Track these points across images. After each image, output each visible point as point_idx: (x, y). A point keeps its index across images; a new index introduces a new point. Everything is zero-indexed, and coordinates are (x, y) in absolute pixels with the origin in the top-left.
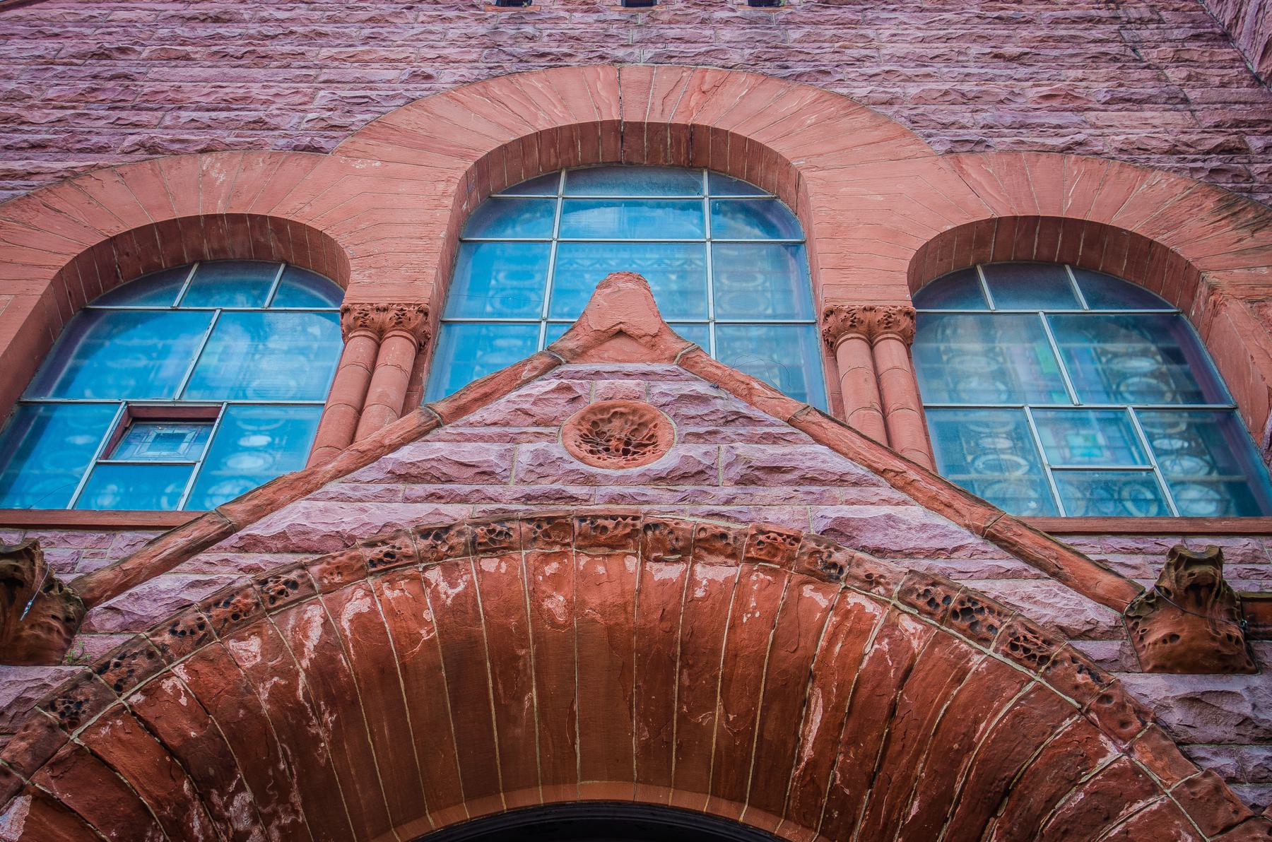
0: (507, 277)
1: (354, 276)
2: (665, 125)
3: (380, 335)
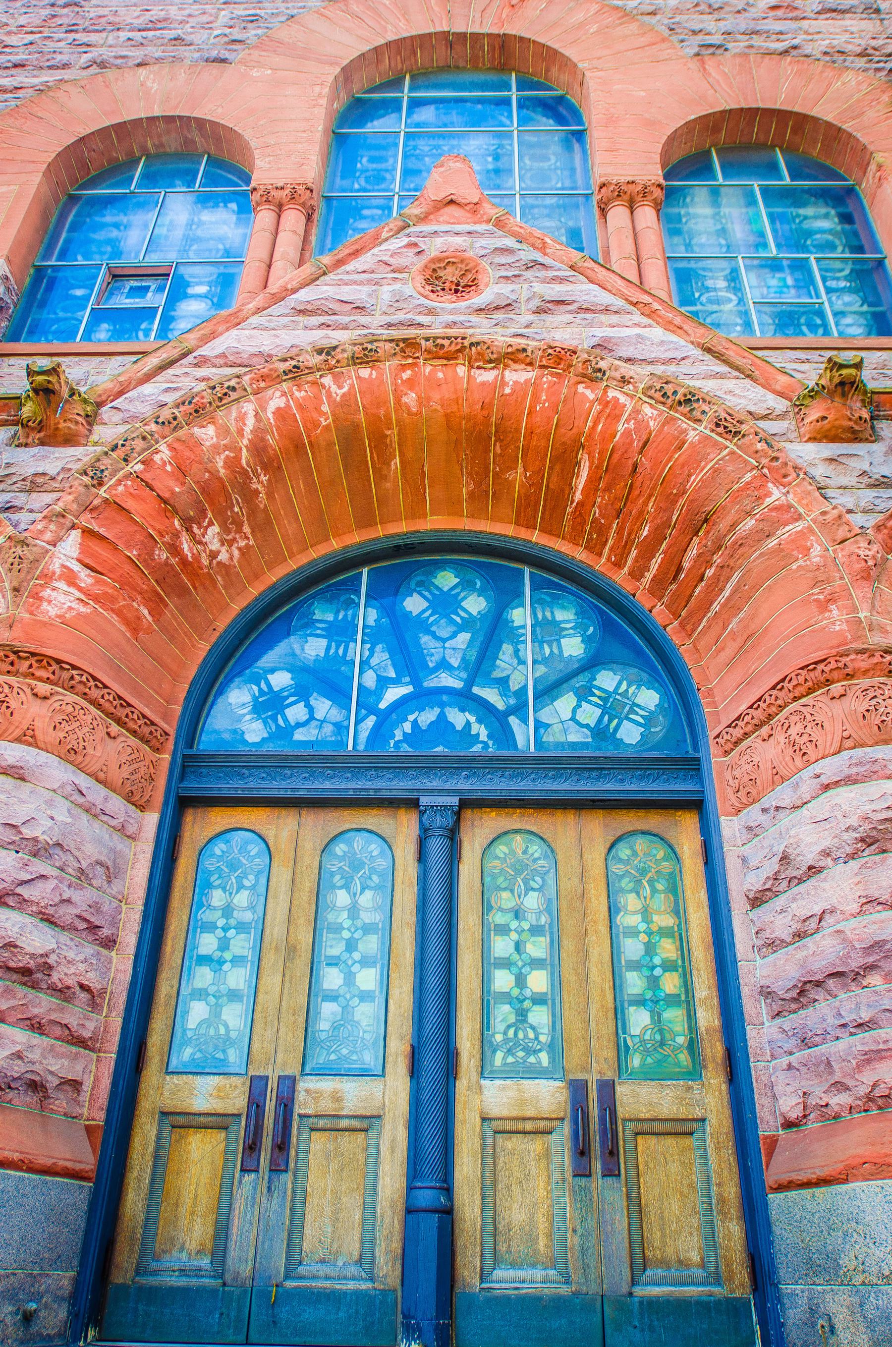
0: (369, 161)
1: (258, 163)
2: (483, 34)
3: (280, 208)
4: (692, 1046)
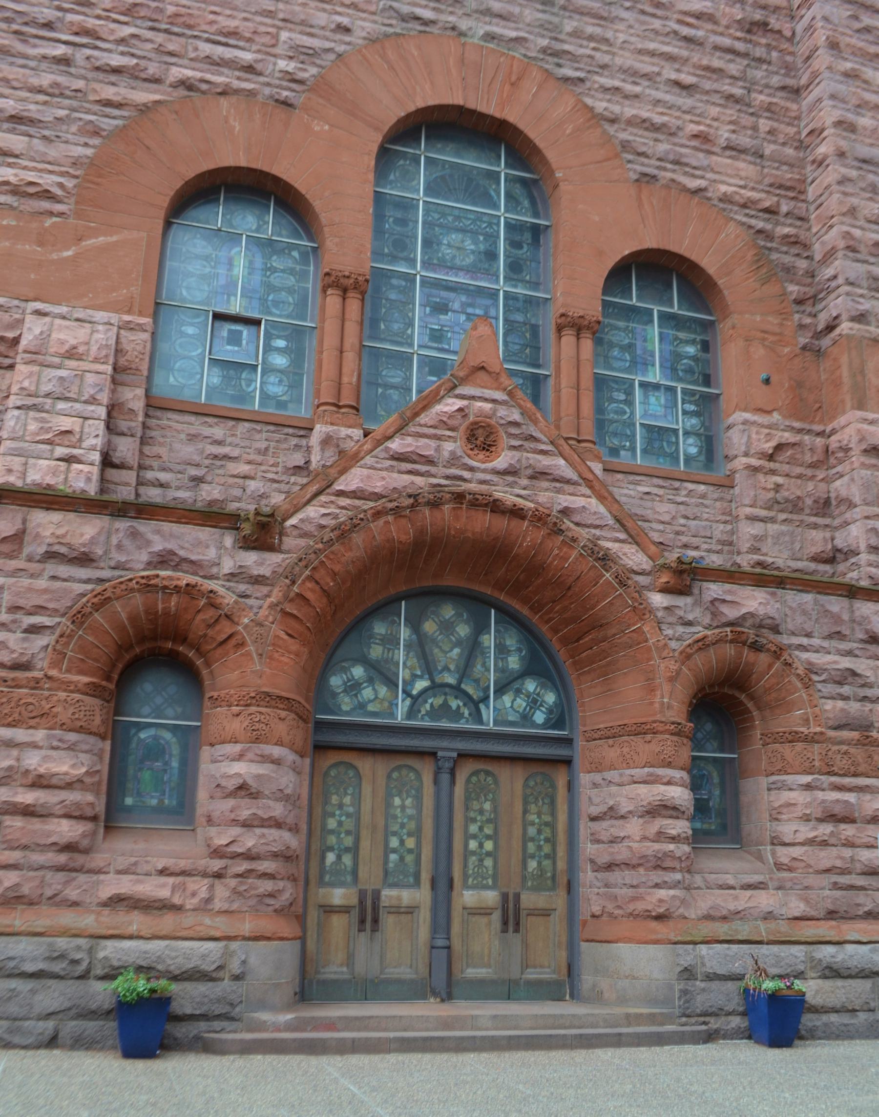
0: (394, 222)
3: (345, 290)
4: (553, 877)
